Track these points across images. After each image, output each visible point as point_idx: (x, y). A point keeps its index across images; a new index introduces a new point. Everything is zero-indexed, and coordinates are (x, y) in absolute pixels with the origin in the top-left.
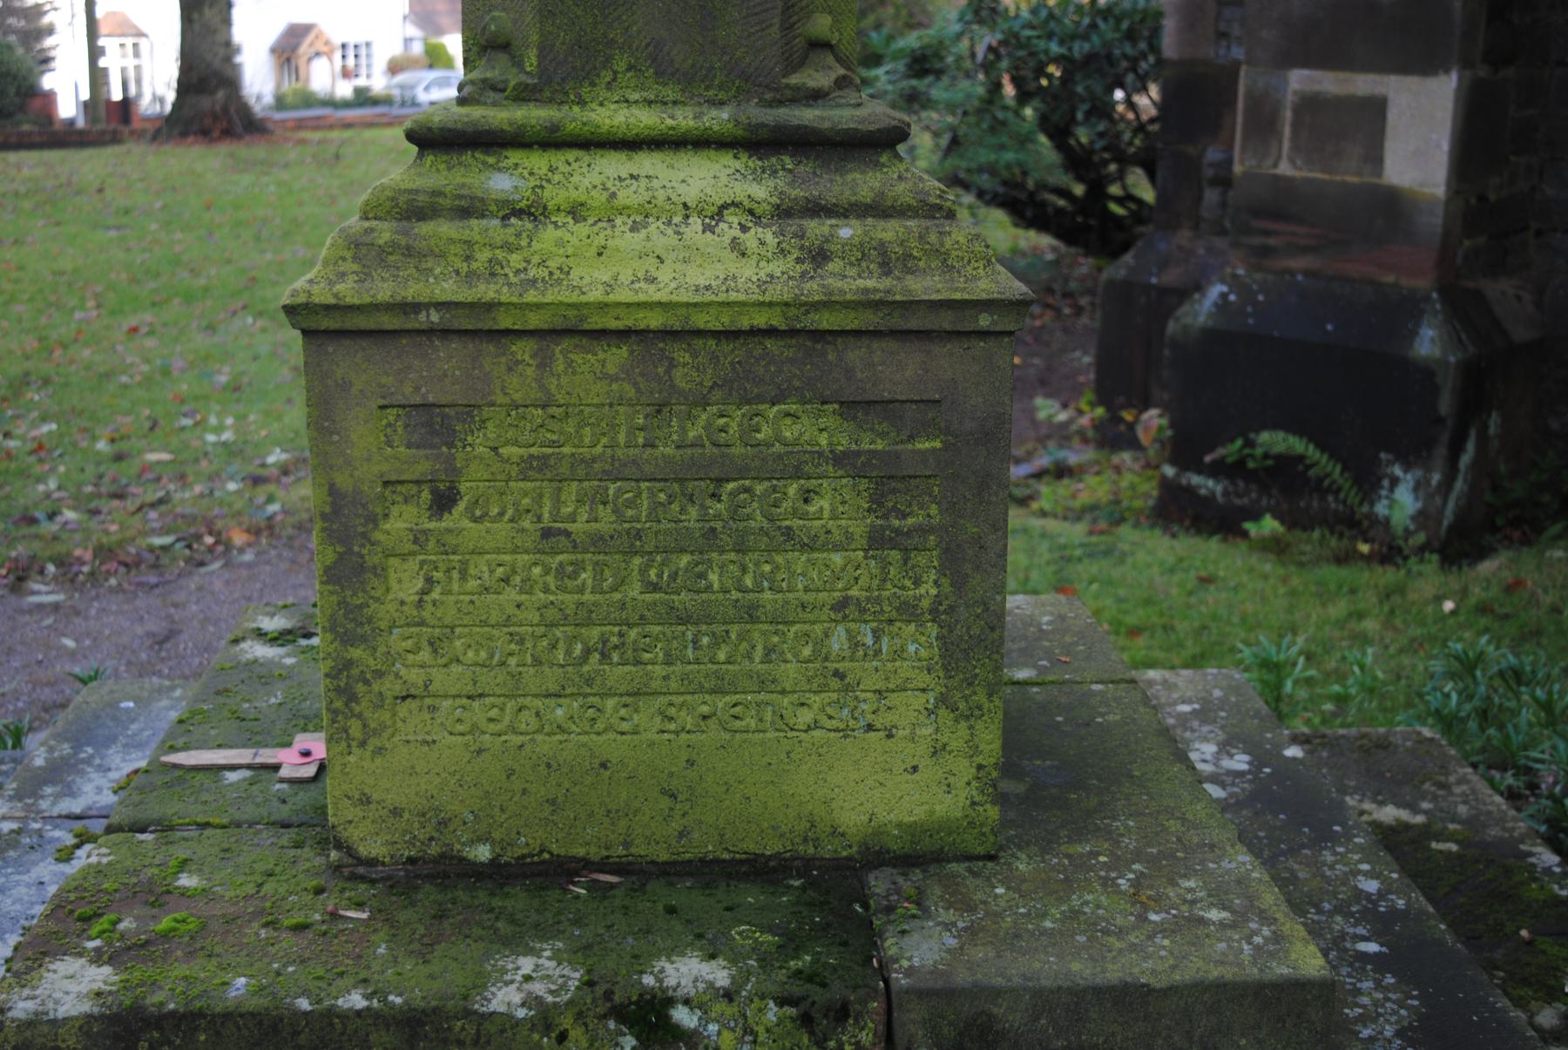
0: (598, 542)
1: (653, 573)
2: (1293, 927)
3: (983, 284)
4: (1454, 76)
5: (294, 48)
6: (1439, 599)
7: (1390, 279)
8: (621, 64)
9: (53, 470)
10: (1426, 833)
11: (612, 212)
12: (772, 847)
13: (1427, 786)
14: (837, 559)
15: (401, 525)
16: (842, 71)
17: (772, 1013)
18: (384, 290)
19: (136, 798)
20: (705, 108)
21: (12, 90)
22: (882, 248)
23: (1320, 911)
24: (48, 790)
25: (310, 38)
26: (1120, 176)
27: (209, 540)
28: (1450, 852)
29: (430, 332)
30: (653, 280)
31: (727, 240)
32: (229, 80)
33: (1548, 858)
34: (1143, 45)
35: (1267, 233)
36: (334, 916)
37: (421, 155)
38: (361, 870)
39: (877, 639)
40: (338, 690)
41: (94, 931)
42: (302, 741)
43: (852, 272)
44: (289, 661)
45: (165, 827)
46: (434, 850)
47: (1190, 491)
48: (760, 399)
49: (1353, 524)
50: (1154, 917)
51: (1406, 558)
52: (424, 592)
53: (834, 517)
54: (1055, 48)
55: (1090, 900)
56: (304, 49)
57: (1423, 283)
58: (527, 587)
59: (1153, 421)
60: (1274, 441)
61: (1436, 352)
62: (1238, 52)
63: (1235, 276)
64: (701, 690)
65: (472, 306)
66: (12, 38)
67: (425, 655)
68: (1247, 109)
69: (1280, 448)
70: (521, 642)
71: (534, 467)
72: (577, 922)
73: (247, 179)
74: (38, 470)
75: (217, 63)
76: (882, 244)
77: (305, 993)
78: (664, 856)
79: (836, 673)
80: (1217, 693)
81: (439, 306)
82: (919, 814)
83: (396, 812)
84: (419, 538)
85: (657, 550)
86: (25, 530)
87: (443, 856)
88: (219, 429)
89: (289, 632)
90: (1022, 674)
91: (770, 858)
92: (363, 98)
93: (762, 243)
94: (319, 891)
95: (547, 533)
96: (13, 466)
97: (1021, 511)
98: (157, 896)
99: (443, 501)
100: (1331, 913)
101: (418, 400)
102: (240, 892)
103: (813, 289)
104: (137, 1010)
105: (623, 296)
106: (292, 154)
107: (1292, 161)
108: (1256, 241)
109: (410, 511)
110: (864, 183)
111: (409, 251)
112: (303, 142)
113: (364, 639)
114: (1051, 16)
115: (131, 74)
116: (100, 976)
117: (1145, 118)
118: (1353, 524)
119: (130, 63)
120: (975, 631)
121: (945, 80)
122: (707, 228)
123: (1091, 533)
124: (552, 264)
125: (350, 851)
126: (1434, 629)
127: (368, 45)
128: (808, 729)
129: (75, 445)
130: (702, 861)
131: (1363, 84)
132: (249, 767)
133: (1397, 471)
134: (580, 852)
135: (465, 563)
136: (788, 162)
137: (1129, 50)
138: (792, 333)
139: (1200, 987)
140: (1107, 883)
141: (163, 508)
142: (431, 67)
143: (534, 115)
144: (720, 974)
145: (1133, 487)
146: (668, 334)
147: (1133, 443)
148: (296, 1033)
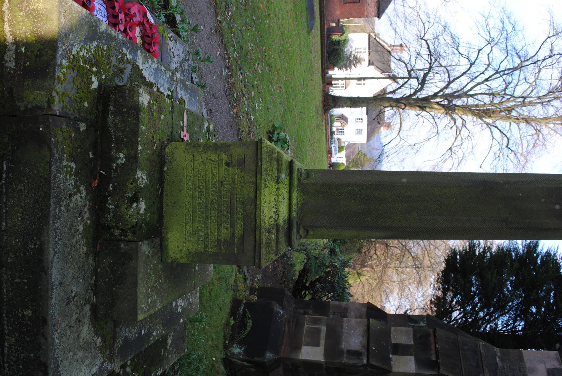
0: (220, 191)
1: (214, 201)
2: (147, 315)
3: (263, 260)
4: (324, 360)
5: (342, 119)
6: (216, 357)
7: (283, 348)
8: (304, 197)
9: (251, 73)
10: (165, 348)
11: (278, 195)
12: (165, 221)
13: (175, 349)
14: (216, 234)
15: (224, 157)
16: (303, 236)
17: (135, 221)
18: (264, 156)
19: (178, 106)
20: (296, 212)
21: (334, 61)
22: (271, 243)
23: (150, 323)
24: (182, 85)
25: (345, 122)
26: (309, 294)
27: (235, 105)
28: (161, 353)
29: (257, 163)
30: (265, 202)
31: (272, 215)
32: (335, 106)
33: (160, 373)
34: (337, 298)
35: (293, 322)
36: (155, 143)
37: (288, 162)
38: (163, 147)
39: (201, 241)
40: (195, 145)
41: (154, 102)
42: (188, 135)
43: (266, 237)
44: (204, 131)
45: (172, 112)
46: (166, 160)
47: (240, 306)
48: (244, 221)
49: (232, 340)
50: (149, 289)
51: (225, 351)
52: (212, 160)
53: (223, 233)
54: (336, 279)
55: (153, 278)
56: (343, 121)
57: (282, 354)
58: (212, 179)
59: (255, 298)
60: (250, 323)
61: (267, 357)
62: (331, 316)
63: (284, 315)
64: (193, 209)
65: (261, 171)
66: (345, 62)
67: (201, 160)
68: (319, 318)
69: (248, 325)
70: (203, 177)
71: (233, 180)
72: (152, 186)
73: (314, 110)
74: (251, 70)
75: (338, 104)
76: (271, 243)
77: (141, 139)
78: (164, 201)
79: (195, 233)
80: (194, 307)
81: (261, 165)
82: (170, 247)
83: (173, 154)
84: (222, 160)
85: (218, 202)
86: (238, 68)
87: (165, 162)
88: (259, 106)
89: (209, 130)
90: (197, 268)
91: (163, 220)
92: (332, 133)
93: (272, 222)
94: (160, 140)
95: (222, 182)
96: (252, 65)
97: (237, 271)
98: (160, 112)
99: (228, 164)
100: (149, 325)
101: (245, 161)
102: (160, 126)
103: (263, 230)
104: (140, 111)
105: (263, 197)
106: (320, 119)
107: (307, 327)
108: (291, 320)
109: (226, 159)
110: (282, 240)
111: (271, 160)
112: (322, 121)
113: (204, 149)
114: (343, 279)
115: (337, 86)
116: (146, 104)
117: (322, 299)
118: (232, 340)
119: (340, 86)
120: (202, 258)
121: (329, 256)
122: (274, 212)
123: (232, 285)
124: (269, 185)
125: (166, 145)
126: (209, 355)
127: (344, 134)
128: (186, 228)
129: (256, 77)
130: (162, 208)
131: (322, 342)
132: (183, 126)
133: (243, 349)
134: (165, 186)
135: (217, 168)
136: (286, 226)
137: (336, 295)
138: (256, 227)
139: (136, 297)
140: (156, 281)
141: (242, 95)
142: (339, 147)
143: (295, 182)
144: (142, 212)
145: (241, 294)
146: (256, 204)
147: (251, 294)
148: (134, 138)
